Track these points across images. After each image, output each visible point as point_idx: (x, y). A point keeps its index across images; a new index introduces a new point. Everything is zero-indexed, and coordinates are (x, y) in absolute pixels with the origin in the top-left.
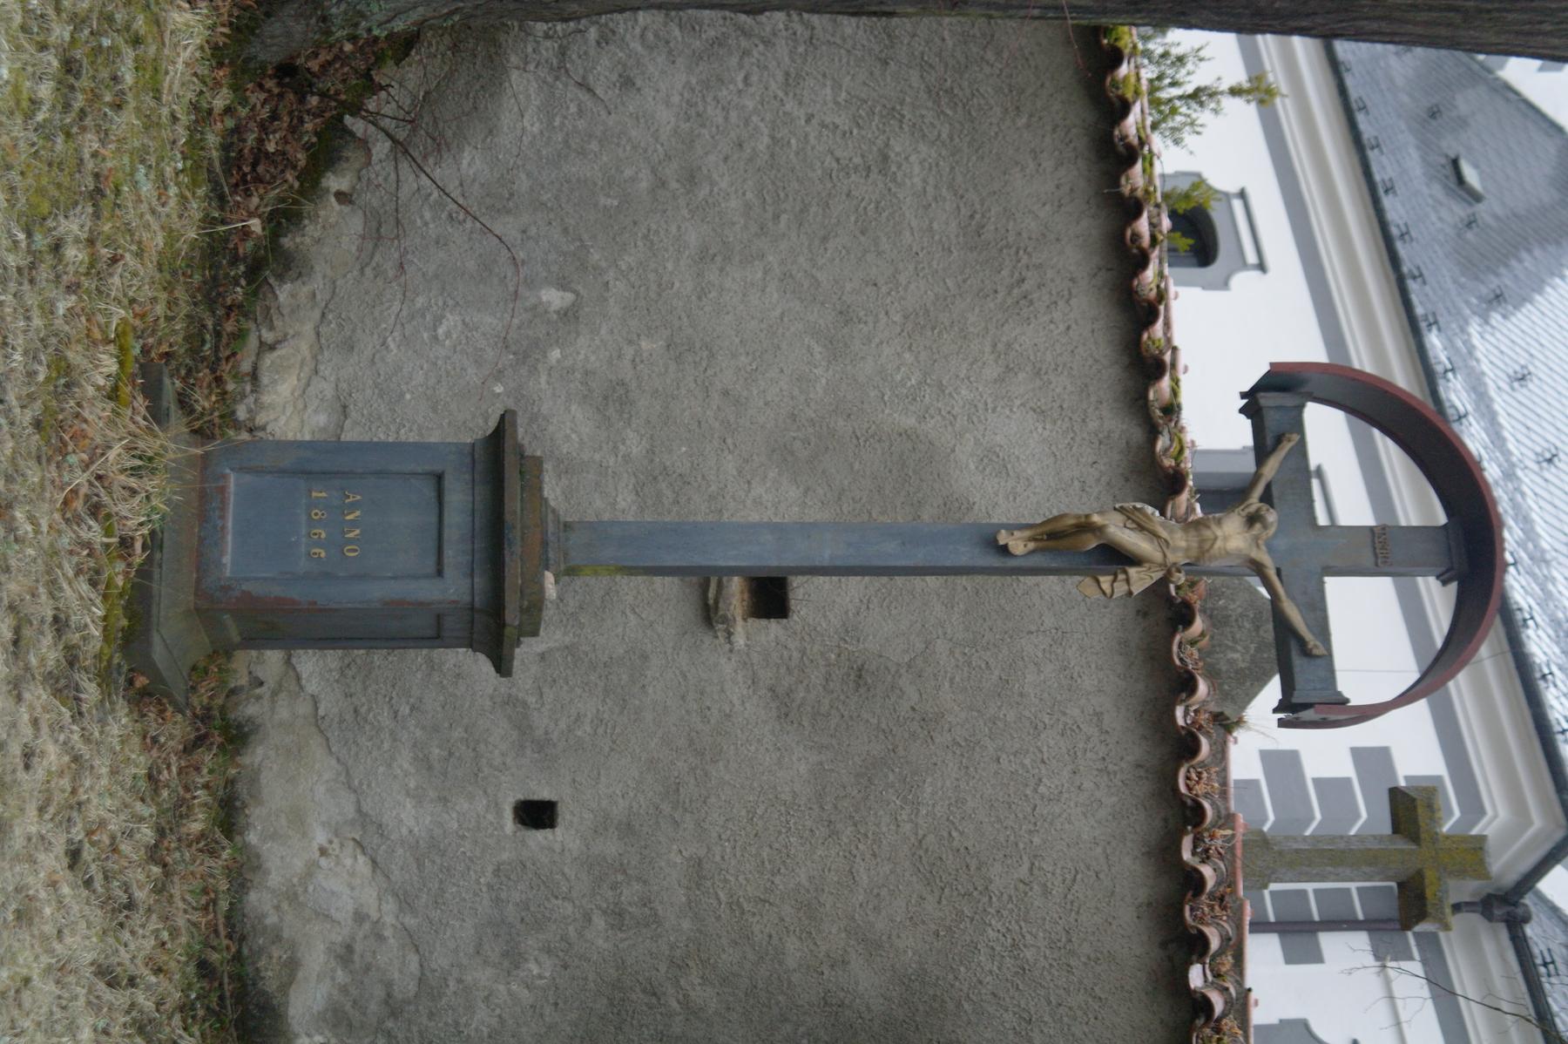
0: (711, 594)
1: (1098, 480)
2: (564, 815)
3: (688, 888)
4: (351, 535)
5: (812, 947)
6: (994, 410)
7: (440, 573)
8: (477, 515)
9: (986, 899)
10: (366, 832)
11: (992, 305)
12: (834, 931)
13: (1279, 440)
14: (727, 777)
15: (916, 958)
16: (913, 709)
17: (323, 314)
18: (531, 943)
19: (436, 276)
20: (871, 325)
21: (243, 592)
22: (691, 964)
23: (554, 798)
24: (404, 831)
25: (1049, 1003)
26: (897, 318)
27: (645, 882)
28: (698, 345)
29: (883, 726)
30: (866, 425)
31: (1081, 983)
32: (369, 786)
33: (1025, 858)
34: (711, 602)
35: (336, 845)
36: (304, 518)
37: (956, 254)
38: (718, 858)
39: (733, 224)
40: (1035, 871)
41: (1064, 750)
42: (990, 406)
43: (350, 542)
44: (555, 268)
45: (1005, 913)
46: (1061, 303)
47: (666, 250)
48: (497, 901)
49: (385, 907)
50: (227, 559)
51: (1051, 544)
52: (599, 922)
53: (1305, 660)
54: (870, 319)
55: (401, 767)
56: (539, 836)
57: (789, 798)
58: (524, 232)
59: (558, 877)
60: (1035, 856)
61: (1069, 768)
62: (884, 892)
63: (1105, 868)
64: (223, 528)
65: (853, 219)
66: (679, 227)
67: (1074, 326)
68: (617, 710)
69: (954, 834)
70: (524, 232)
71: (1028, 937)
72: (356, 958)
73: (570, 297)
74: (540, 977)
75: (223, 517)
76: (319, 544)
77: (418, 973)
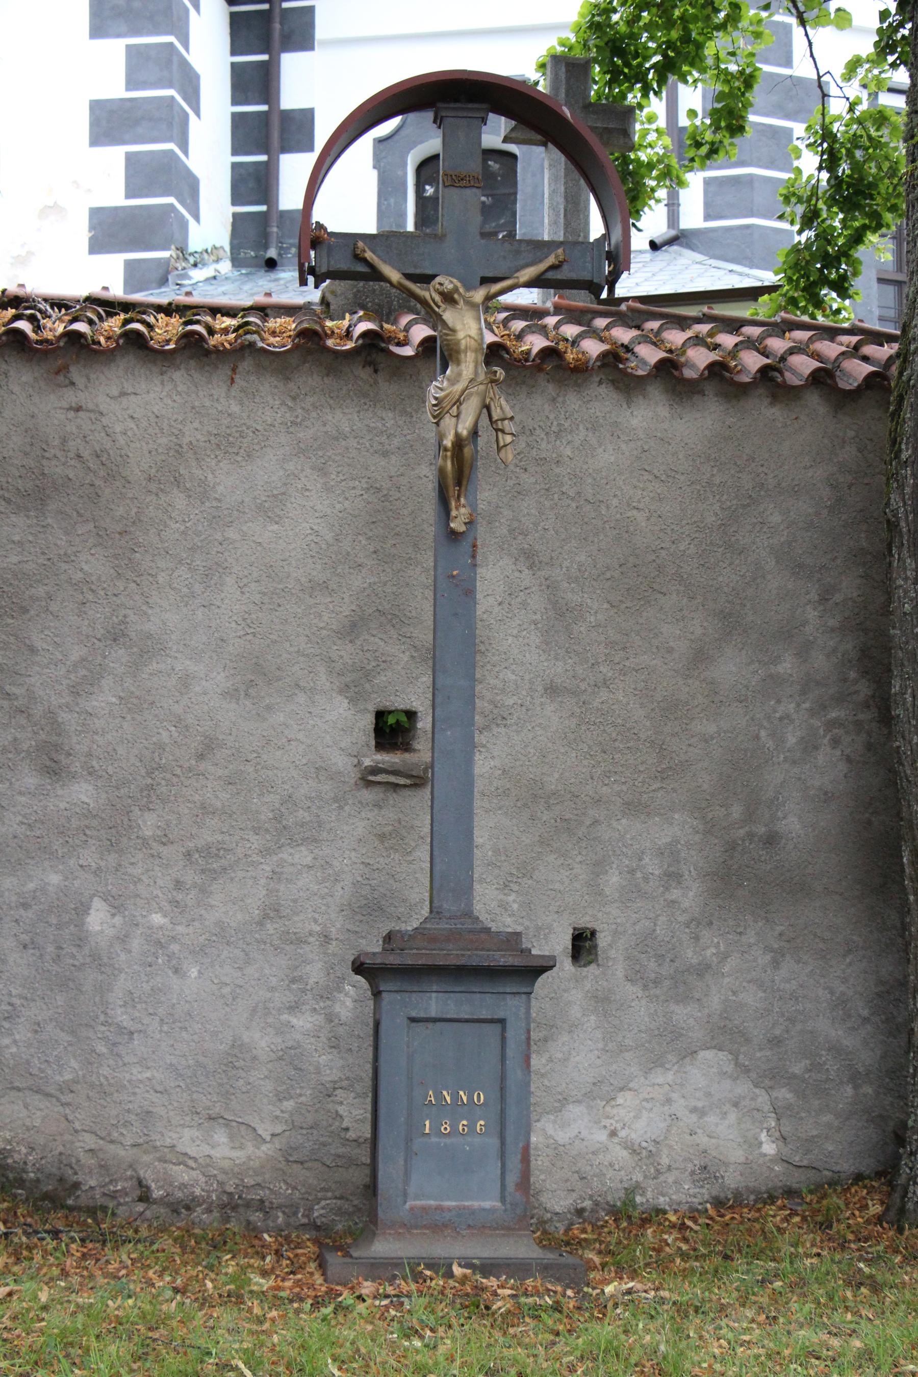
0: (402, 781)
1: (290, 408)
2: (585, 922)
3: (649, 814)
4: (448, 1099)
5: (698, 710)
6: (219, 501)
7: (502, 1022)
8: (409, 989)
9: (663, 553)
10: (601, 1093)
11: (108, 491)
12: (687, 689)
13: (358, 258)
14: (556, 775)
15: (710, 618)
16: (500, 604)
17: (112, 1142)
18: (690, 955)
19: (73, 1032)
20: (128, 612)
21: (516, 1190)
22: (710, 816)
23: (519, 929)
24: (599, 1062)
25: (748, 505)
26: (120, 584)
27: (643, 853)
28: (149, 781)
29: (515, 632)
30: (233, 625)
31: (733, 476)
32: (560, 1093)
33: (629, 514)
34: (408, 782)
35: (607, 1122)
36: (448, 1141)
37: (50, 521)
38: (624, 788)
39: (15, 739)
40: (641, 506)
41: (538, 469)
42: (215, 504)
43: (470, 1098)
44: (66, 918)
45: (675, 536)
46: (105, 421)
47: (46, 807)
48: (656, 982)
49: (660, 1080)
50: (487, 1204)
51: (464, 483)
52: (675, 894)
53: (565, 267)
54: (123, 612)
55: (544, 1065)
56: (603, 940)
57: (574, 721)
58: (25, 947)
59: (637, 928)
60: (629, 505)
61: (554, 466)
62: (655, 642)
63: (639, 443)
64: (459, 1208)
65: (10, 621)
66: (20, 793)
67: (130, 412)
68: (497, 871)
69: (608, 575)
70: (25, 947)
71: (695, 519)
72: (700, 1104)
73: (97, 903)
74: (717, 946)
75: (449, 1209)
76: (472, 1126)
77: (715, 1051)
